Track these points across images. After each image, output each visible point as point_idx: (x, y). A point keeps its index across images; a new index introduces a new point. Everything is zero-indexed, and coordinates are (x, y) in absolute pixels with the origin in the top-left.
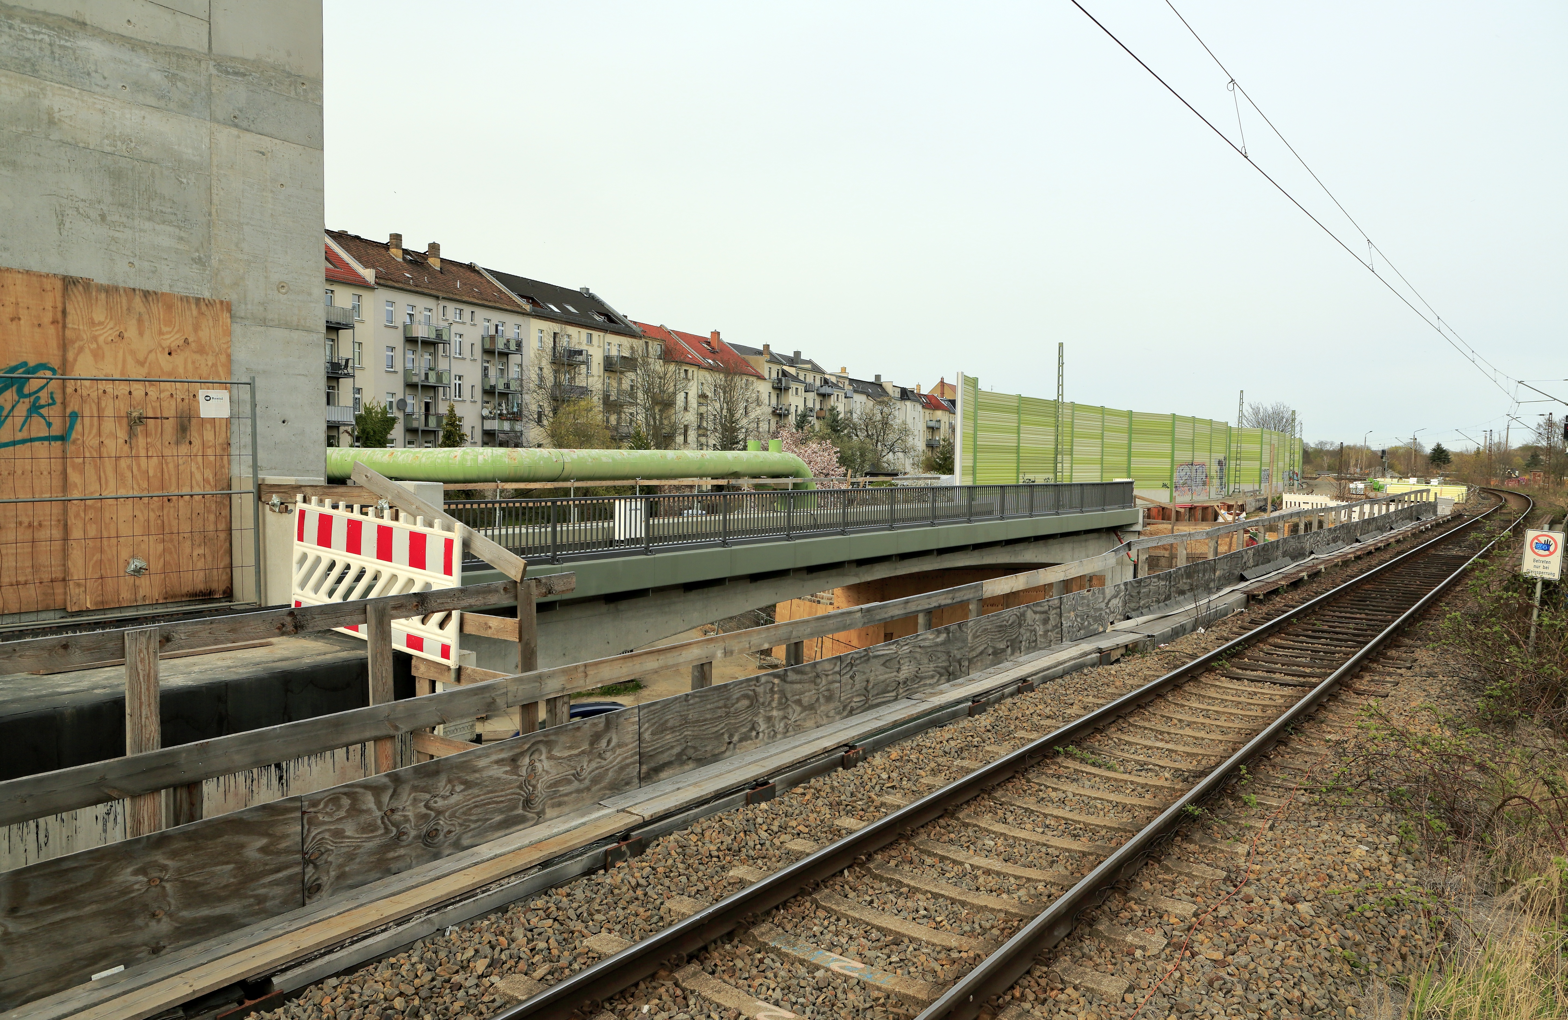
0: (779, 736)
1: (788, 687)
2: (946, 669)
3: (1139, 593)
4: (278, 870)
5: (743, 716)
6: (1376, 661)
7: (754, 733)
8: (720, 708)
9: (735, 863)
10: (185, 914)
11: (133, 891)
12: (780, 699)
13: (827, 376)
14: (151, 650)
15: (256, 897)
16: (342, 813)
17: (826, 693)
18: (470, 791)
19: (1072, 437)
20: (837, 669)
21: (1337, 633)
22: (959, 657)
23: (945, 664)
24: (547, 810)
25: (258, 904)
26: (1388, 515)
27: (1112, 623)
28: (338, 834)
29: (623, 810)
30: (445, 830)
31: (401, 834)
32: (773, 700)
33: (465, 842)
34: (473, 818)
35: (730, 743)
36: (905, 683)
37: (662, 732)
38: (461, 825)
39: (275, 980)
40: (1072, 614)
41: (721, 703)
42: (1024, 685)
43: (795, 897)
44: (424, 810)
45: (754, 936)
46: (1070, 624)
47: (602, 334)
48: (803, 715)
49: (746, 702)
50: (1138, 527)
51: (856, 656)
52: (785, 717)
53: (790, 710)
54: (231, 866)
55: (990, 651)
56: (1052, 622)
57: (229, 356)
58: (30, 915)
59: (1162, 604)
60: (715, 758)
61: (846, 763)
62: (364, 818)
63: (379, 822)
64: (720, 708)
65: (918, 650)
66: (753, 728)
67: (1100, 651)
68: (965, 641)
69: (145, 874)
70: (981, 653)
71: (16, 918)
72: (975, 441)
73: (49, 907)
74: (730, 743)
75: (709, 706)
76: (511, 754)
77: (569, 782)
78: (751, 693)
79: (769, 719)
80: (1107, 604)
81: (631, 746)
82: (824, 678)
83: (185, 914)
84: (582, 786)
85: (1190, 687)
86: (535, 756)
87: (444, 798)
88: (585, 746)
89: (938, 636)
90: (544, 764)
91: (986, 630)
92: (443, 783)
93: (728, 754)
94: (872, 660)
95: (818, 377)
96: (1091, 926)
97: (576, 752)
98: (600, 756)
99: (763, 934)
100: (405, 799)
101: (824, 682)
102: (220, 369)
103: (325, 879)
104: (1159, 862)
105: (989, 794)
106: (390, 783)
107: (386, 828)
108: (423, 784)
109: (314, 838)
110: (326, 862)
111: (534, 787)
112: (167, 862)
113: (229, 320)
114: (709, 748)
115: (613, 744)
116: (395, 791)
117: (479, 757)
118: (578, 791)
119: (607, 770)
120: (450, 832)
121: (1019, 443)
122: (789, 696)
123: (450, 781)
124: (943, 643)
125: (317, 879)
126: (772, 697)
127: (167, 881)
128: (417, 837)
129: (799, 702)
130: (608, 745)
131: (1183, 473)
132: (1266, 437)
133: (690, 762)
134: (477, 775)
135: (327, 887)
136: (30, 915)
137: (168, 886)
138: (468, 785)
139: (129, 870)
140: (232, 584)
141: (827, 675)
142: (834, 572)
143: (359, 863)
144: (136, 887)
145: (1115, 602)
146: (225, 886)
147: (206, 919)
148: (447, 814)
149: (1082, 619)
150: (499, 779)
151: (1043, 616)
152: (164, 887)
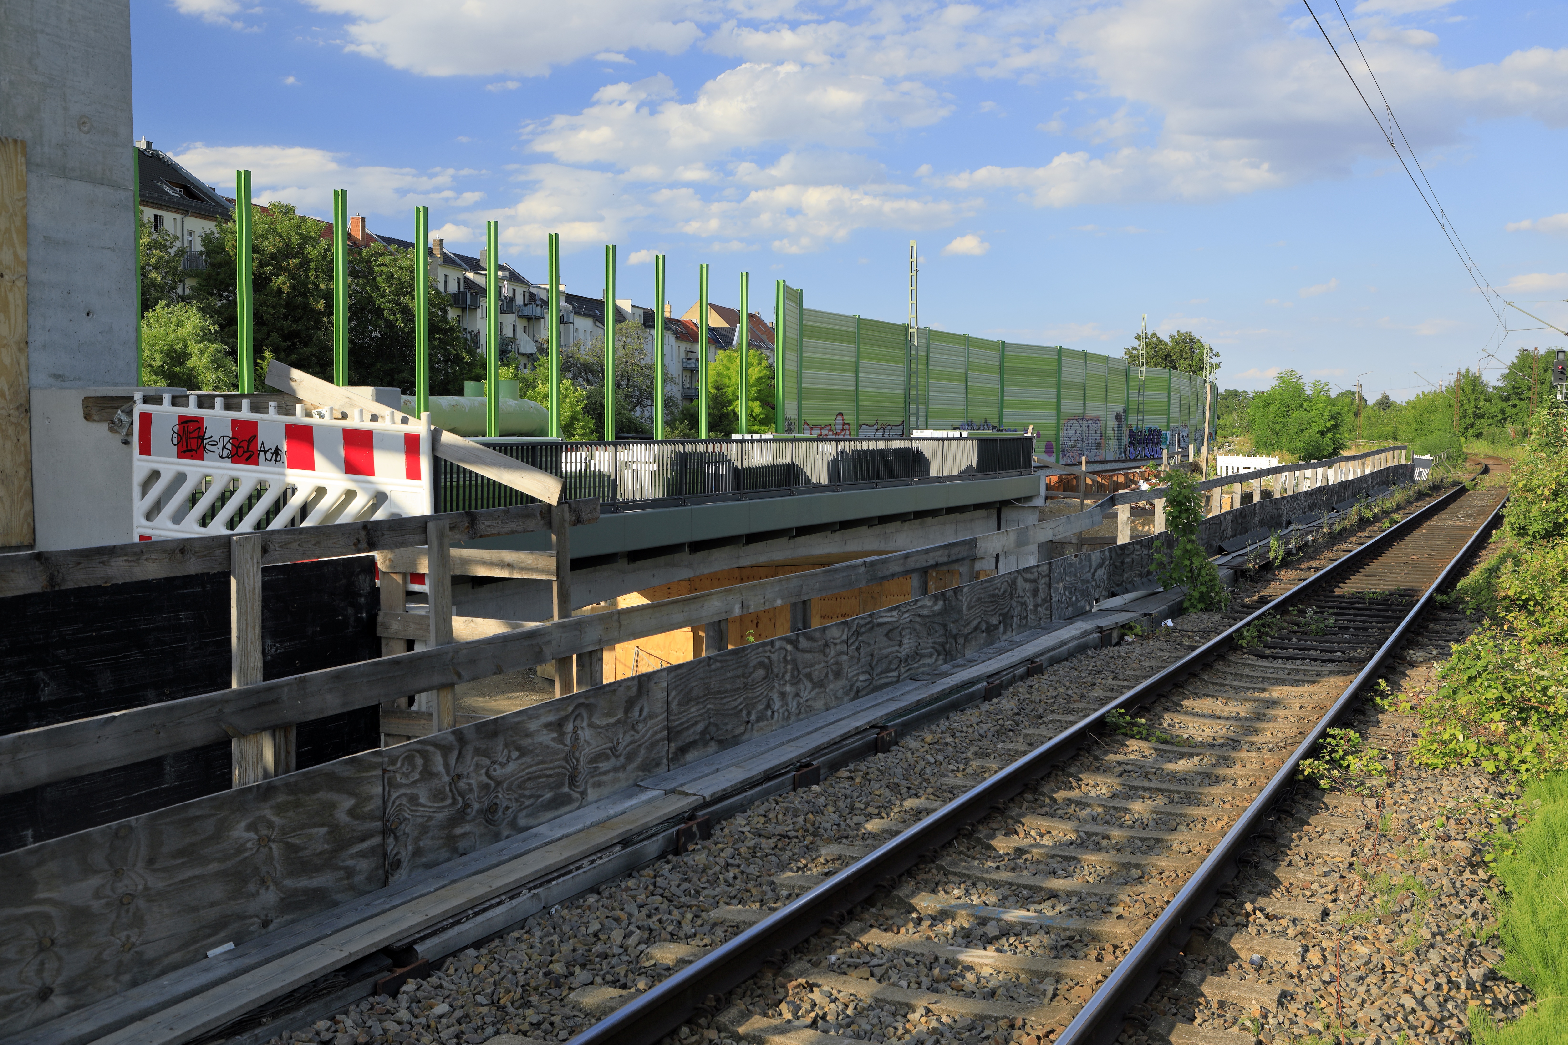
0: (793, 718)
1: (799, 655)
2: (943, 645)
3: (1122, 563)
4: (363, 840)
5: (759, 690)
6: (1419, 634)
7: (769, 712)
8: (738, 677)
9: (818, 843)
10: (289, 883)
11: (246, 850)
12: (793, 670)
13: (534, 290)
14: (255, 561)
15: (345, 868)
16: (416, 776)
17: (834, 667)
18: (523, 760)
19: (928, 378)
20: (845, 637)
21: (1359, 609)
22: (955, 632)
23: (942, 640)
24: (590, 791)
25: (348, 878)
26: (1363, 479)
27: (1097, 601)
28: (413, 799)
29: (673, 791)
30: (504, 805)
31: (467, 806)
32: (786, 672)
33: (522, 822)
34: (527, 793)
35: (748, 722)
36: (906, 660)
37: (688, 703)
38: (517, 800)
39: (418, 948)
40: (1061, 585)
41: (740, 672)
42: (1032, 668)
43: (916, 865)
44: (484, 779)
45: (900, 898)
46: (1058, 598)
47: (178, 217)
48: (813, 693)
49: (761, 672)
50: (1039, 502)
51: (862, 622)
52: (797, 695)
53: (802, 686)
54: (325, 830)
55: (984, 627)
56: (1041, 595)
57: (25, 218)
58: (165, 870)
59: (1144, 579)
60: (735, 741)
61: (878, 746)
62: (435, 783)
63: (448, 789)
64: (738, 677)
65: (918, 619)
66: (768, 706)
67: (1100, 629)
68: (960, 612)
69: (256, 831)
70: (976, 628)
71: (154, 870)
72: (800, 382)
73: (180, 861)
74: (748, 722)
75: (729, 675)
76: (557, 717)
77: (607, 758)
78: (766, 661)
79: (783, 695)
80: (1094, 574)
81: (660, 718)
82: (832, 646)
83: (289, 883)
84: (618, 764)
85: (1219, 666)
86: (578, 722)
87: (503, 765)
88: (620, 715)
89: (935, 604)
90: (586, 734)
91: (980, 599)
92: (501, 748)
93: (746, 736)
94: (876, 629)
95: (520, 290)
96: (1257, 868)
97: (612, 720)
98: (633, 728)
99: (907, 896)
100: (468, 763)
101: (833, 653)
102: (15, 236)
103: (404, 854)
104: (1292, 815)
105: (1063, 770)
106: (455, 743)
107: (454, 798)
108: (484, 746)
109: (394, 803)
110: (404, 834)
111: (578, 760)
112: (275, 819)
113: (24, 167)
114: (729, 727)
115: (645, 714)
116: (460, 753)
117: (531, 718)
118: (615, 769)
119: (640, 746)
120: (507, 808)
121: (857, 386)
122: (800, 667)
123: (506, 745)
124: (940, 614)
125: (397, 853)
126: (785, 667)
127: (274, 841)
128: (480, 811)
129: (809, 676)
130: (640, 715)
131: (1072, 432)
132: (1175, 380)
133: (713, 743)
134: (529, 741)
135: (405, 864)
136: (165, 870)
137: (274, 846)
138: (523, 752)
139: (243, 824)
140: (34, 540)
141: (835, 644)
142: (662, 560)
143: (432, 838)
144: (249, 845)
145: (1100, 572)
146: (321, 853)
147: (306, 891)
148: (505, 786)
149: (1070, 593)
150: (548, 747)
151: (1033, 585)
152: (271, 848)
